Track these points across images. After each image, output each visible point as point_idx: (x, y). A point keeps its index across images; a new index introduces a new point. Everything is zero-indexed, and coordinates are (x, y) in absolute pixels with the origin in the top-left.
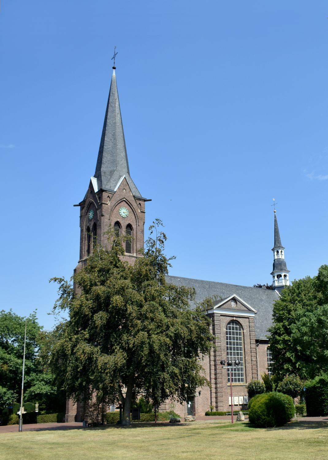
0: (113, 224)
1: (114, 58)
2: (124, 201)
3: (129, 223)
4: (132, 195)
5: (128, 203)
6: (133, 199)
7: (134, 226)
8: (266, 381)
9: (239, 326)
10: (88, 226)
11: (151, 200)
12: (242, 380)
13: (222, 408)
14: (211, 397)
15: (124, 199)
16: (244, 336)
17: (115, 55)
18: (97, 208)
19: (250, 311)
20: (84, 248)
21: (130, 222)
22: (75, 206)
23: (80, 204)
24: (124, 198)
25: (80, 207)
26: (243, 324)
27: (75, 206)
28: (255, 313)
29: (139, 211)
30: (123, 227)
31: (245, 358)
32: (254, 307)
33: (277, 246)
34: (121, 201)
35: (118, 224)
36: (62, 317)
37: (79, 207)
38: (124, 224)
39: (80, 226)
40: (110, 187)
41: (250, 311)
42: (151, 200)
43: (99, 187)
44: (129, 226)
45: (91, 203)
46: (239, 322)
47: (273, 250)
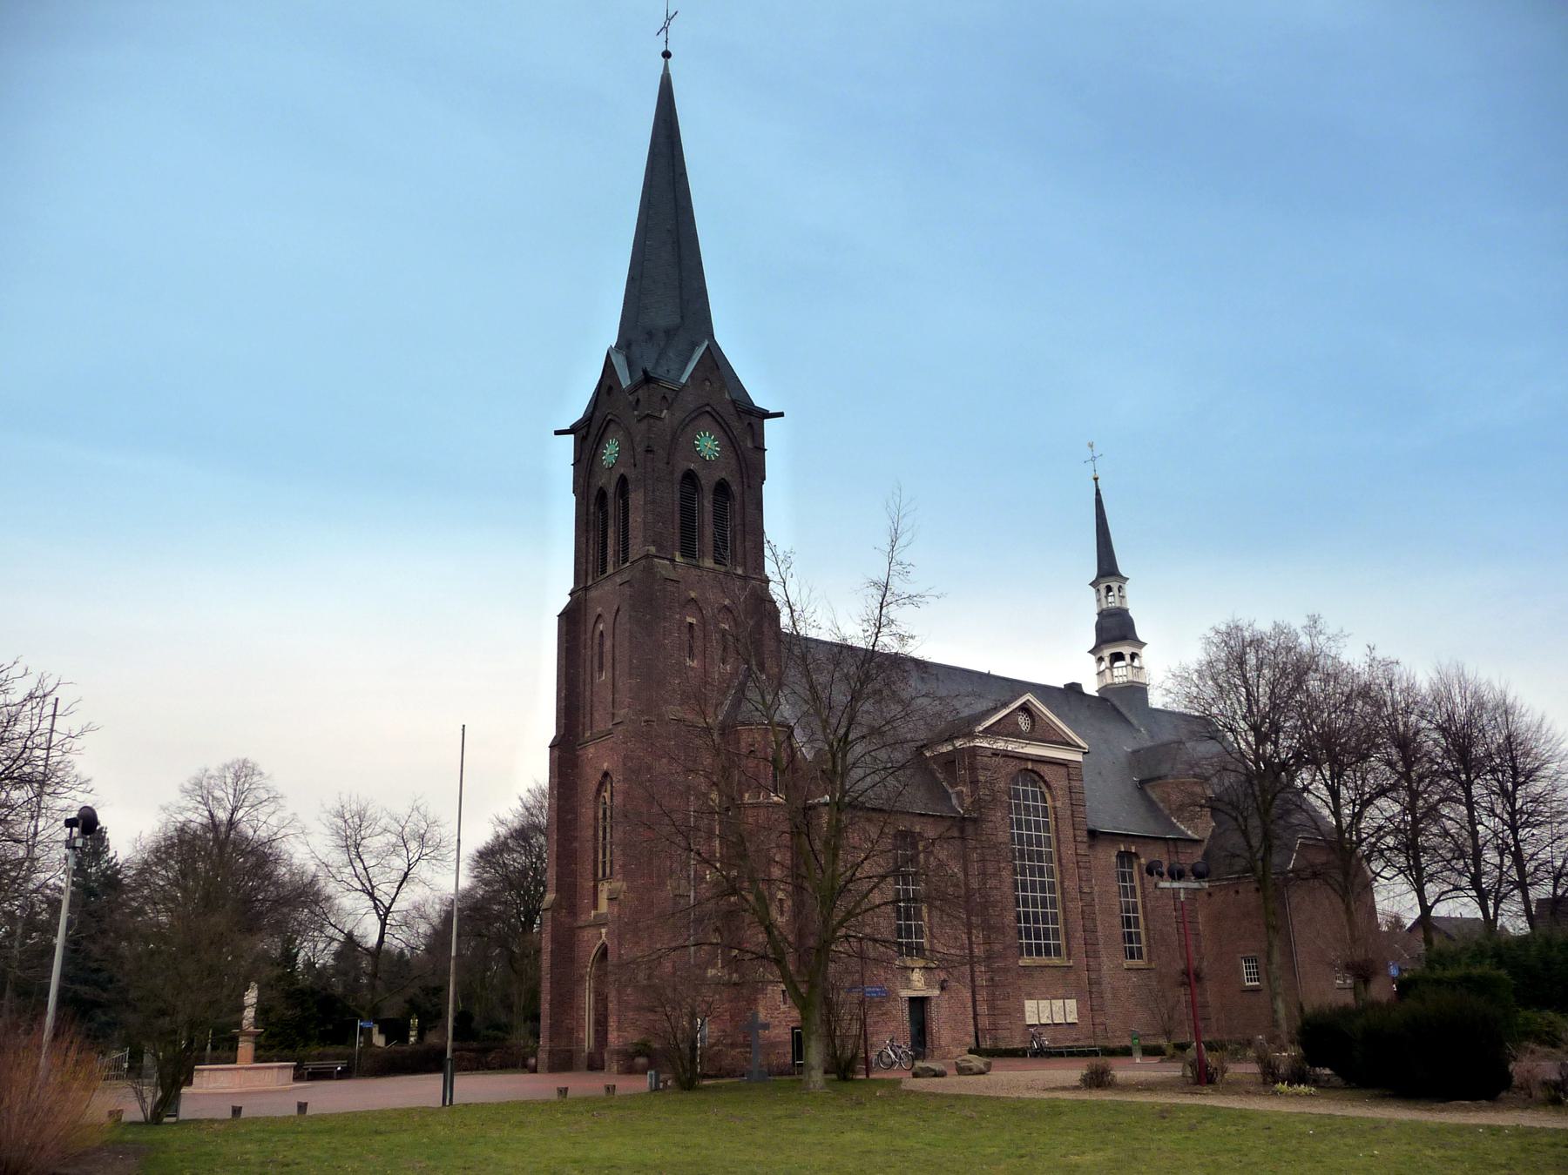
0: (678, 475)
1: (665, 28)
6: (732, 410)
7: (735, 488)
8: (133, 995)
11: (781, 415)
12: (1058, 953)
13: (1006, 1033)
14: (974, 1002)
17: (669, 19)
18: (684, 380)
21: (723, 475)
22: (557, 433)
23: (571, 431)
25: (572, 437)
26: (1054, 784)
27: (557, 433)
29: (750, 445)
30: (706, 488)
31: (1062, 883)
32: (1083, 738)
33: (1108, 569)
34: (700, 412)
35: (690, 478)
36: (1098, 474)
38: (707, 480)
41: (1067, 744)
42: (781, 415)
44: (722, 488)
46: (1041, 777)
47: (1094, 584)
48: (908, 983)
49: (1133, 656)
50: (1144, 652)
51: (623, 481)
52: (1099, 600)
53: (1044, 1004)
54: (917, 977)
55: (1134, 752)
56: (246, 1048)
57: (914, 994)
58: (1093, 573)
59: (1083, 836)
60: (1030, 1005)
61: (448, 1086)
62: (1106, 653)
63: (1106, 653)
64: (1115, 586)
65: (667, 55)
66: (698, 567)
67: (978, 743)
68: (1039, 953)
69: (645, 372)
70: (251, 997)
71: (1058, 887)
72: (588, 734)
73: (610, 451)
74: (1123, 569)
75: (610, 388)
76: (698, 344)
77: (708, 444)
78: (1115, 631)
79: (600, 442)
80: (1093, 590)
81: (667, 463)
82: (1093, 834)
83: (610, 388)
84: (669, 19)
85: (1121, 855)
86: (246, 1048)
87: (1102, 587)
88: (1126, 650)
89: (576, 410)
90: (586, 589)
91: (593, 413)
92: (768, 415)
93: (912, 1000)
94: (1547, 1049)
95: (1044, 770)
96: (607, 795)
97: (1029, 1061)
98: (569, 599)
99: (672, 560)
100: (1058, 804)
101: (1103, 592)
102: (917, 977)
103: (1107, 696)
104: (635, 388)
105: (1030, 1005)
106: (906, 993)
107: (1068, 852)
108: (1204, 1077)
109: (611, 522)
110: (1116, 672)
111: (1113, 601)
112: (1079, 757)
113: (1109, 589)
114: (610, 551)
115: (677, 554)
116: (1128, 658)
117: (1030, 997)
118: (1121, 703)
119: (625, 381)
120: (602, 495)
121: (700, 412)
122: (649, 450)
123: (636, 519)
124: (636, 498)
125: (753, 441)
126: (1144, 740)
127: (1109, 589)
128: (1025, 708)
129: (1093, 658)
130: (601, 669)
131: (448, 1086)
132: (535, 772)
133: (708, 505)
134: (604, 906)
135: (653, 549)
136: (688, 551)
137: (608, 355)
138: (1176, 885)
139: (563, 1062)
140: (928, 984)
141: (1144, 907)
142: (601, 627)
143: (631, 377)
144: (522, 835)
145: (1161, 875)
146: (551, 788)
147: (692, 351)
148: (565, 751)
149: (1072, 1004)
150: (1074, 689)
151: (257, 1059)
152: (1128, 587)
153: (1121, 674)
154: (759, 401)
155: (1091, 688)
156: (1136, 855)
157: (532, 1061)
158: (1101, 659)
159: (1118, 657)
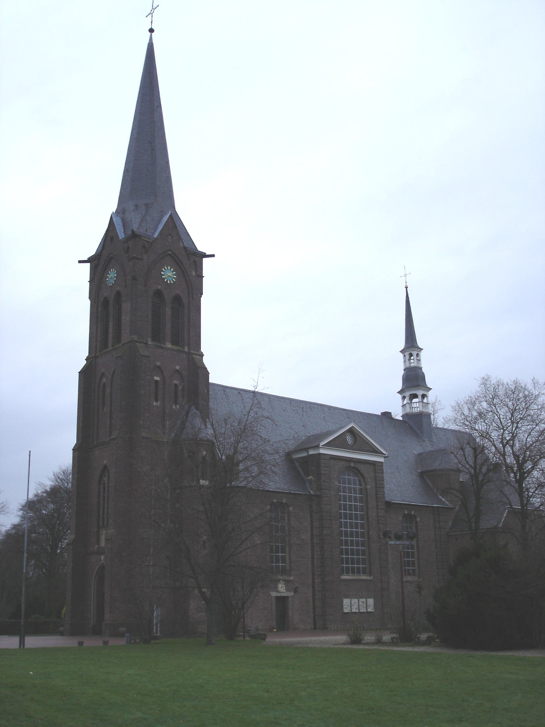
1: (151, 14)
2: (169, 254)
3: (178, 294)
4: (181, 245)
5: (176, 258)
7: (185, 300)
9: (358, 477)
10: (105, 298)
11: (213, 256)
12: (364, 573)
15: (170, 253)
16: (367, 495)
17: (153, 9)
19: (376, 452)
20: (100, 309)
22: (80, 262)
24: (170, 250)
25: (89, 264)
27: (80, 262)
28: (385, 457)
35: (158, 294)
37: (88, 265)
39: (98, 263)
40: (147, 230)
41: (376, 452)
42: (213, 256)
43: (281, 436)
45: (112, 257)
46: (359, 471)
48: (276, 589)
49: (424, 396)
50: (430, 394)
51: (118, 295)
52: (405, 362)
53: (355, 601)
54: (281, 587)
55: (419, 455)
57: (279, 595)
58: (402, 344)
60: (346, 602)
61: (22, 642)
62: (407, 394)
63: (407, 394)
64: (415, 353)
65: (151, 31)
66: (162, 347)
67: (322, 451)
68: (353, 573)
69: (133, 232)
71: (287, 559)
72: (95, 443)
73: (112, 275)
74: (420, 343)
75: (112, 238)
76: (166, 214)
77: (169, 274)
79: (105, 270)
80: (402, 355)
81: (145, 276)
82: (389, 504)
83: (112, 238)
84: (153, 9)
85: (405, 516)
87: (407, 354)
88: (420, 393)
89: (92, 251)
90: (96, 357)
91: (101, 251)
92: (205, 255)
93: (278, 598)
95: (361, 467)
96: (106, 479)
98: (85, 362)
99: (146, 344)
100: (368, 487)
101: (407, 357)
102: (281, 587)
103: (406, 420)
104: (127, 240)
105: (346, 602)
106: (274, 594)
108: (356, 640)
109: (111, 319)
110: (414, 405)
111: (413, 363)
112: (381, 460)
113: (411, 355)
114: (110, 336)
115: (149, 339)
116: (420, 397)
117: (347, 597)
118: (416, 424)
119: (121, 235)
120: (106, 302)
122: (134, 278)
123: (126, 318)
124: (126, 306)
125: (196, 272)
126: (428, 447)
127: (411, 355)
128: (351, 431)
129: (400, 396)
130: (104, 405)
131: (22, 642)
132: (65, 460)
133: (168, 311)
134: (103, 544)
135: (135, 338)
136: (157, 335)
137: (111, 218)
138: (397, 543)
139: (77, 630)
140: (288, 590)
141: (418, 546)
142: (104, 380)
143: (125, 232)
144: (54, 493)
145: (390, 538)
146: (73, 467)
148: (81, 451)
149: (371, 601)
150: (387, 415)
152: (422, 354)
153: (417, 406)
154: (201, 247)
155: (398, 415)
156: (415, 517)
157: (62, 629)
158: (404, 398)
159: (415, 396)
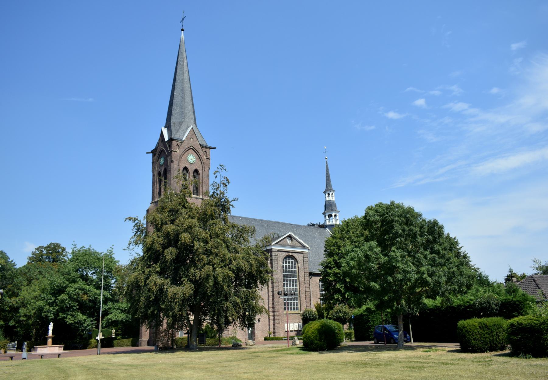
0: (181, 169)
11: (215, 148)
13: (279, 334)
14: (269, 324)
22: (147, 153)
25: (151, 154)
27: (147, 153)
32: (307, 244)
33: (328, 189)
34: (189, 149)
35: (186, 169)
38: (191, 169)
42: (215, 148)
44: (196, 171)
56: (50, 341)
59: (307, 274)
70: (51, 327)
78: (329, 207)
86: (50, 341)
94: (84, 364)
95: (295, 255)
97: (269, 341)
101: (327, 195)
107: (302, 279)
116: (333, 216)
121: (189, 149)
147: (187, 129)
151: (53, 344)
